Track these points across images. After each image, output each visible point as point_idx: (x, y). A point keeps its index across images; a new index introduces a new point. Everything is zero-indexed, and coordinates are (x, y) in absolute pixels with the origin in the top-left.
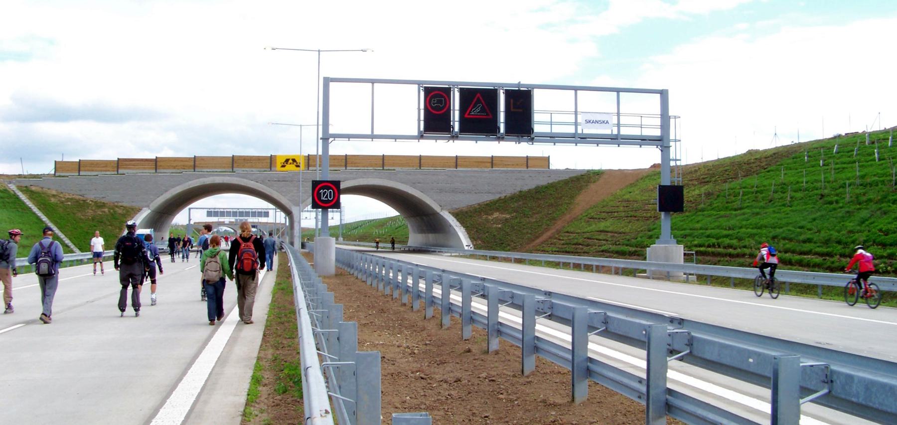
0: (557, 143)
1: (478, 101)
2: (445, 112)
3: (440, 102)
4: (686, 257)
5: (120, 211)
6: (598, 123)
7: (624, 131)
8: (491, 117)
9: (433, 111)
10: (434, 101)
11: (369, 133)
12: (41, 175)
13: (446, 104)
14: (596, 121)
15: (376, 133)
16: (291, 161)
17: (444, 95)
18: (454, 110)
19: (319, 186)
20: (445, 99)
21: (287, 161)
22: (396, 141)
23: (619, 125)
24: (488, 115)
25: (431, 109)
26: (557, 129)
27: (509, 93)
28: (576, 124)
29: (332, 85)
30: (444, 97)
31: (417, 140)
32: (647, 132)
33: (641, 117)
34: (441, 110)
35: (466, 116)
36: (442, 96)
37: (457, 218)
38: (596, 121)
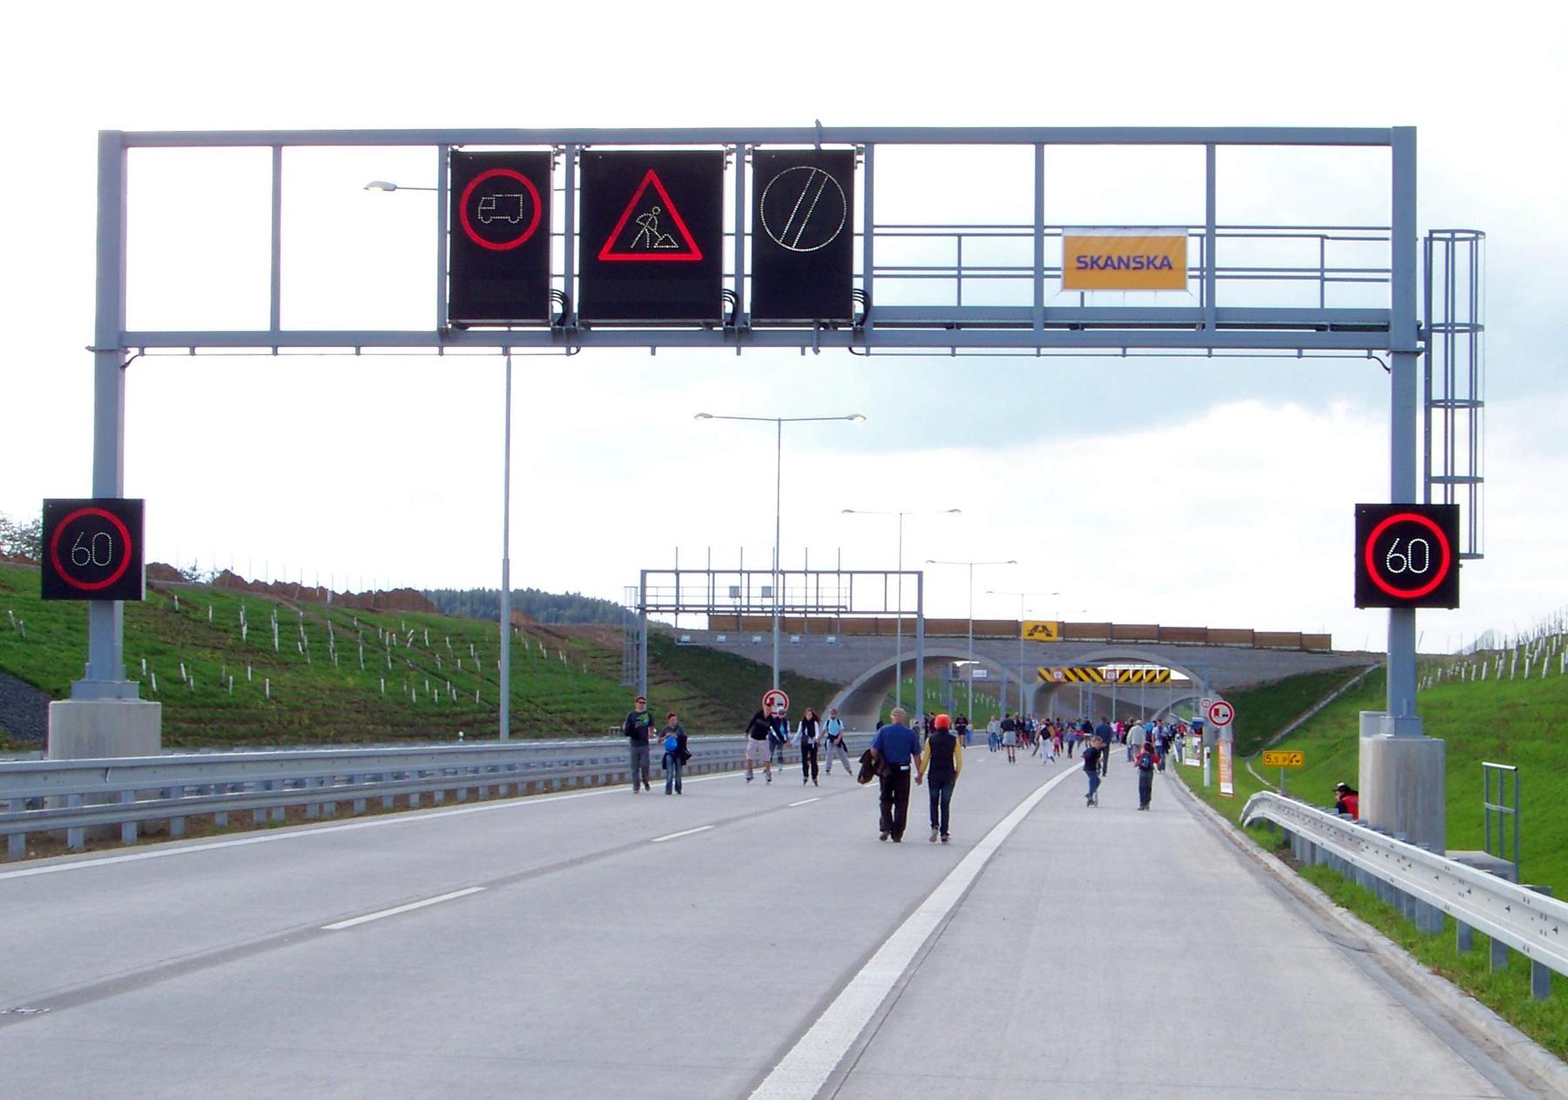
0: (958, 346)
1: (651, 199)
2: (531, 240)
3: (508, 207)
4: (143, 687)
5: (32, 854)
6: (1127, 267)
7: (1230, 295)
8: (697, 256)
9: (492, 246)
10: (489, 203)
11: (265, 326)
12: (951, 909)
13: (473, 201)
14: (1120, 259)
15: (285, 326)
16: (1040, 629)
17: (523, 179)
18: (569, 234)
19: (116, 576)
20: (528, 198)
21: (1036, 628)
22: (358, 353)
23: (1209, 273)
24: (684, 248)
25: (476, 238)
26: (980, 294)
27: (767, 166)
28: (1039, 272)
29: (136, 158)
30: (525, 190)
31: (436, 350)
32: (1345, 298)
33: (1323, 237)
34: (515, 236)
35: (605, 255)
36: (517, 186)
37: (512, 722)
38: (1120, 259)
